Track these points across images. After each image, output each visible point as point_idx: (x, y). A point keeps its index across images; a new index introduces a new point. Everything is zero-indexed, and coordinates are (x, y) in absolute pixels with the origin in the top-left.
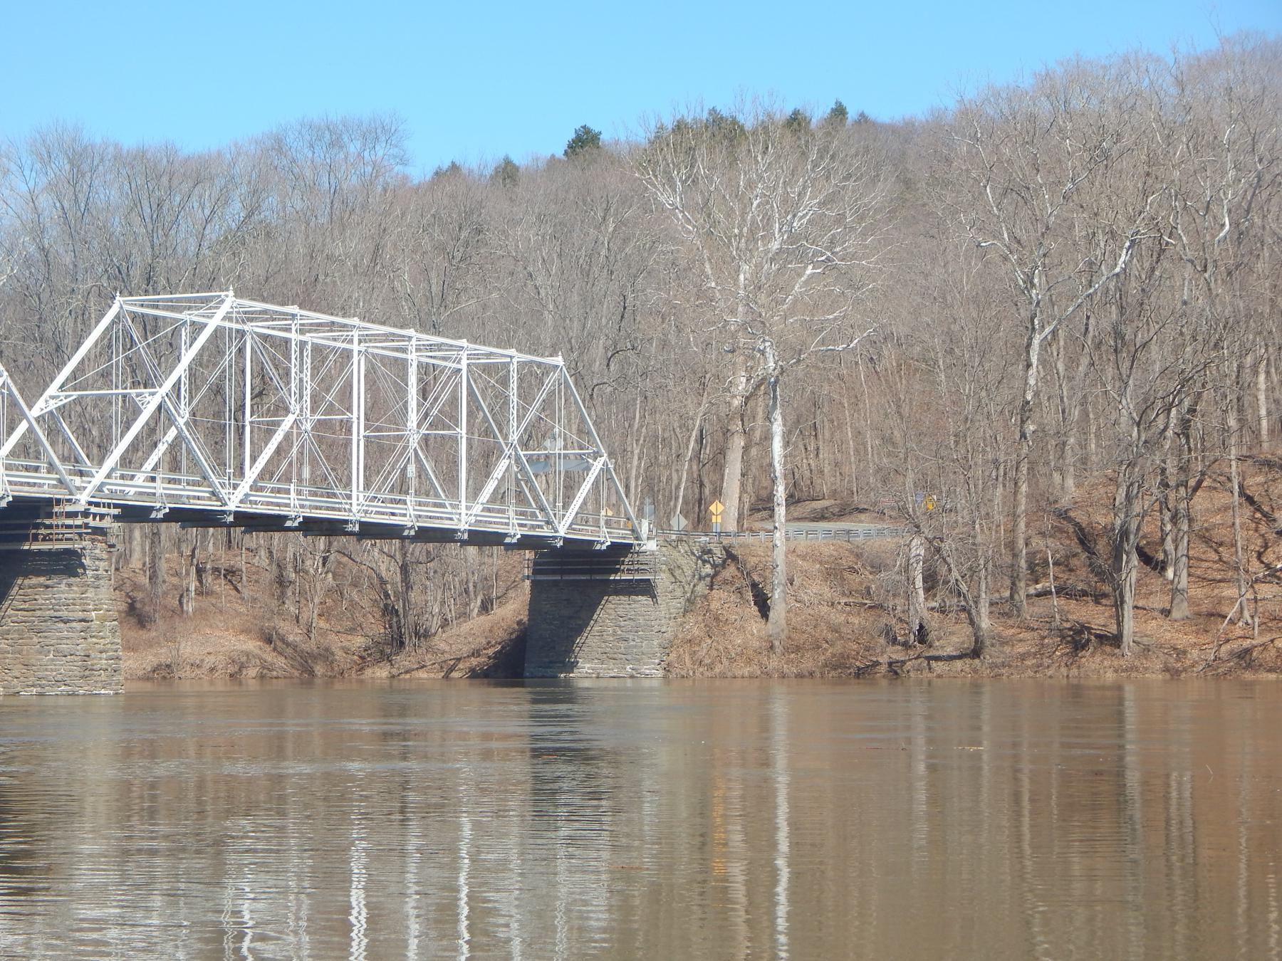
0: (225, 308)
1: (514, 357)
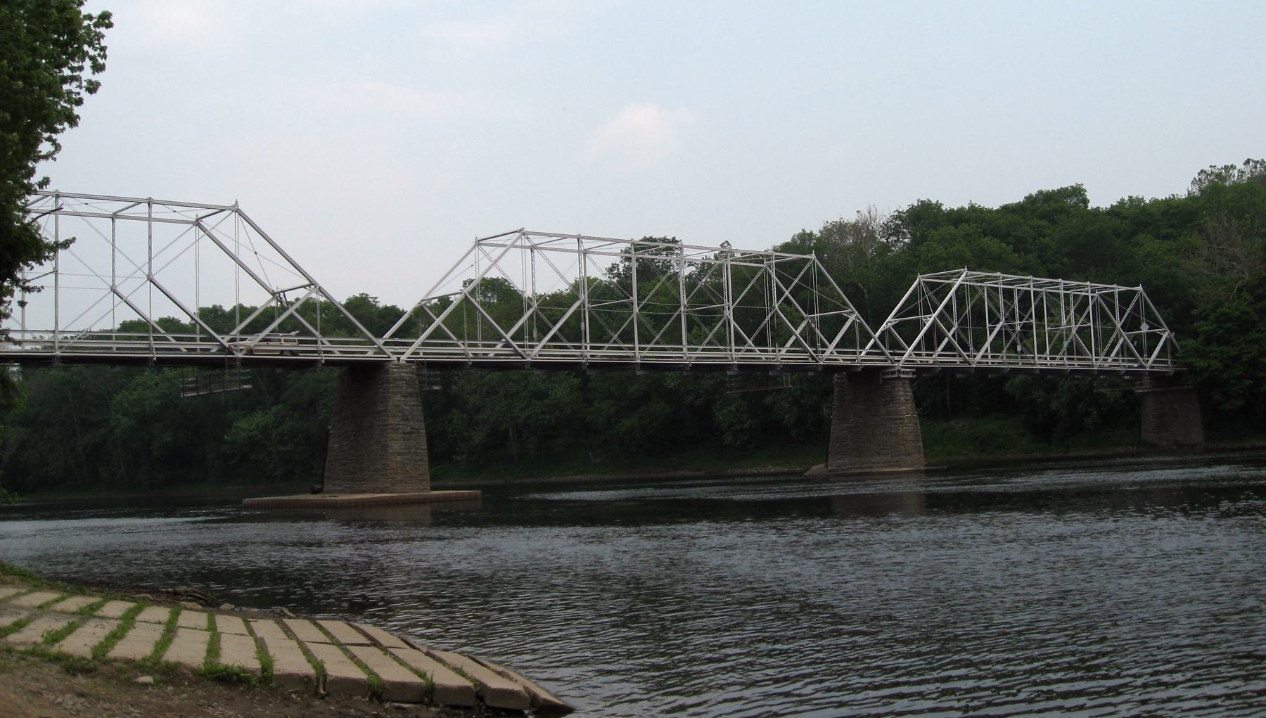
0: (963, 277)
1: (1117, 289)
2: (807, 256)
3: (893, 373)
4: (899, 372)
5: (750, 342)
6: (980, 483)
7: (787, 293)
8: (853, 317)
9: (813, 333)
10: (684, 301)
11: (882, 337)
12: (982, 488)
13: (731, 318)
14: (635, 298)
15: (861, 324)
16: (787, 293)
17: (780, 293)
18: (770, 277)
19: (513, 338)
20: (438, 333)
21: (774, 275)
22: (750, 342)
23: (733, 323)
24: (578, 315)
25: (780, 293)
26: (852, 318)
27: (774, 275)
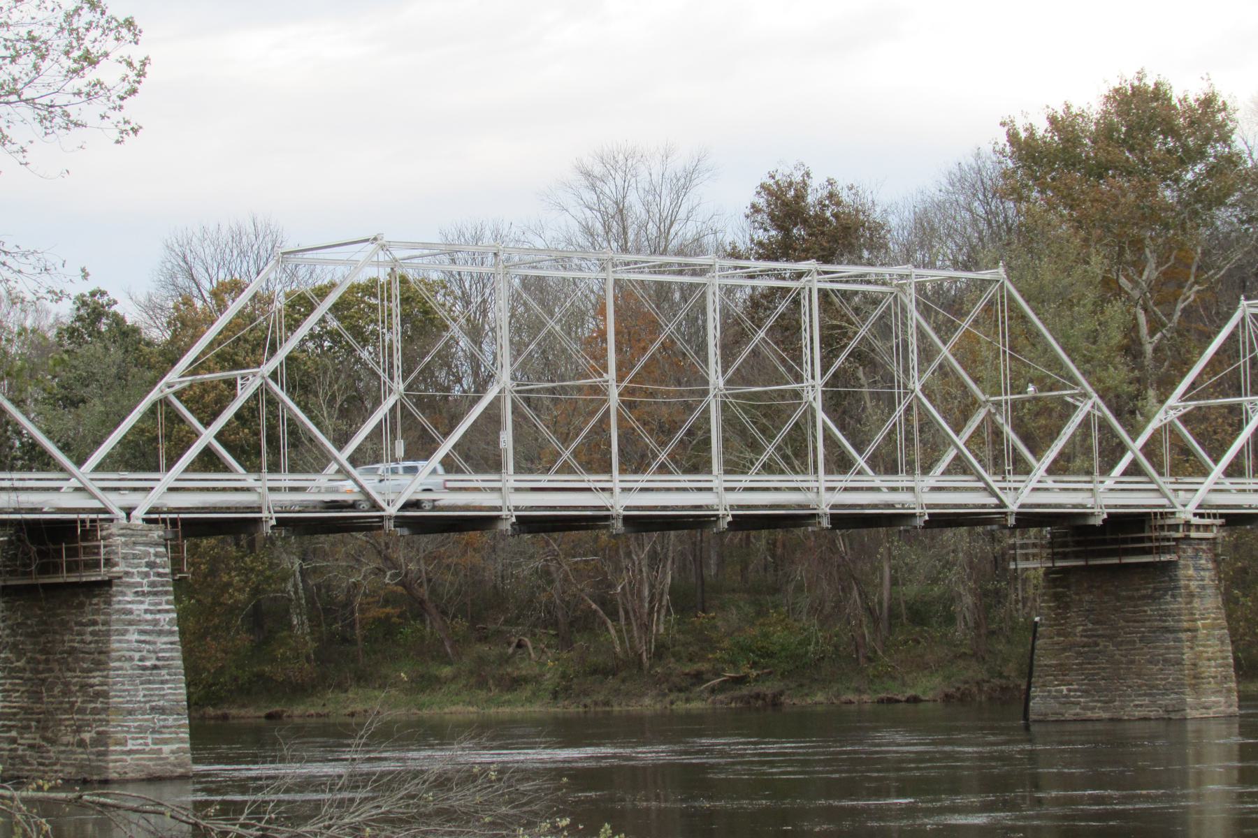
2: (985, 275)
3: (1175, 527)
4: (1188, 525)
5: (861, 462)
6: (598, 759)
7: (945, 351)
8: (1090, 405)
9: (998, 433)
10: (716, 379)
11: (1150, 450)
12: (590, 751)
13: (818, 405)
14: (612, 374)
15: (1104, 426)
16: (945, 351)
17: (927, 353)
18: (904, 310)
19: (353, 460)
20: (208, 461)
21: (912, 307)
22: (861, 462)
23: (821, 416)
24: (492, 418)
25: (927, 353)
26: (1084, 408)
27: (912, 307)
